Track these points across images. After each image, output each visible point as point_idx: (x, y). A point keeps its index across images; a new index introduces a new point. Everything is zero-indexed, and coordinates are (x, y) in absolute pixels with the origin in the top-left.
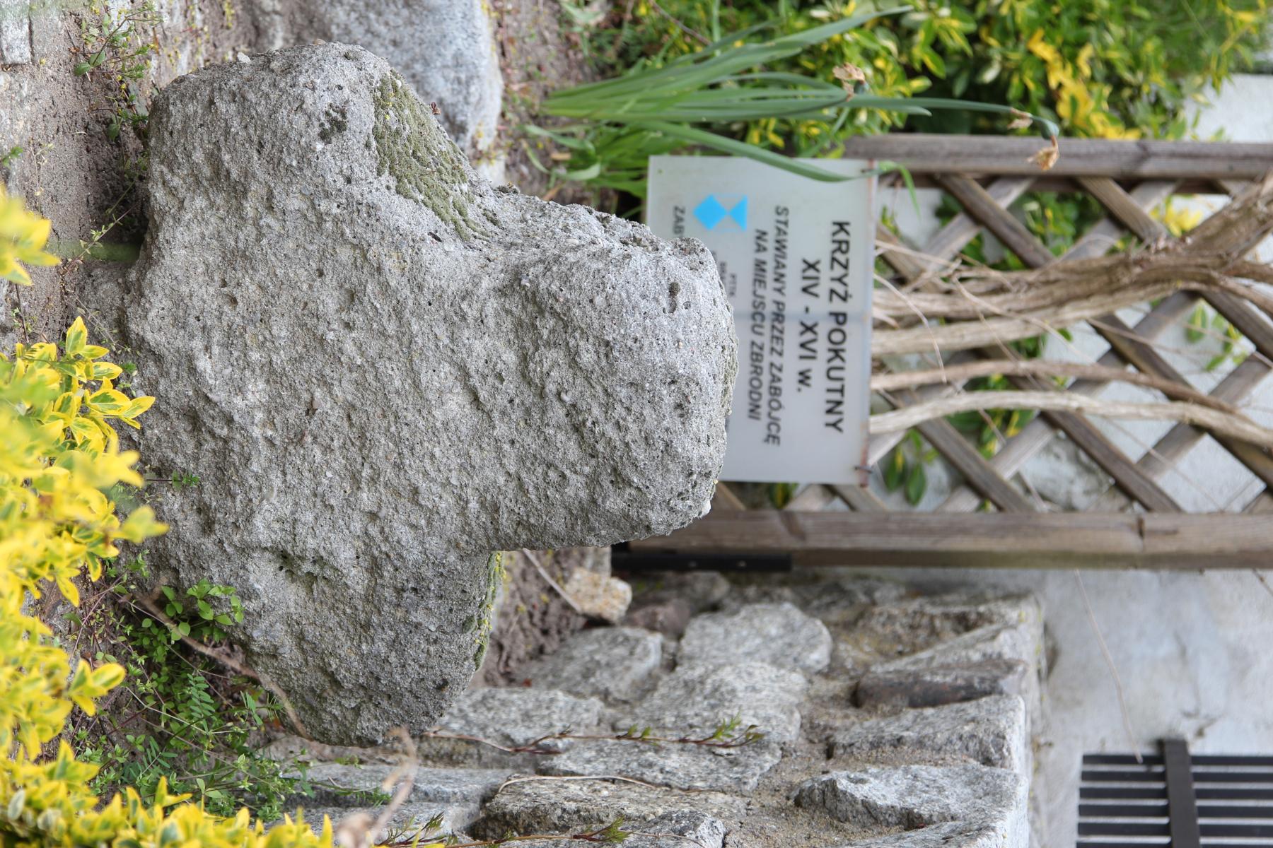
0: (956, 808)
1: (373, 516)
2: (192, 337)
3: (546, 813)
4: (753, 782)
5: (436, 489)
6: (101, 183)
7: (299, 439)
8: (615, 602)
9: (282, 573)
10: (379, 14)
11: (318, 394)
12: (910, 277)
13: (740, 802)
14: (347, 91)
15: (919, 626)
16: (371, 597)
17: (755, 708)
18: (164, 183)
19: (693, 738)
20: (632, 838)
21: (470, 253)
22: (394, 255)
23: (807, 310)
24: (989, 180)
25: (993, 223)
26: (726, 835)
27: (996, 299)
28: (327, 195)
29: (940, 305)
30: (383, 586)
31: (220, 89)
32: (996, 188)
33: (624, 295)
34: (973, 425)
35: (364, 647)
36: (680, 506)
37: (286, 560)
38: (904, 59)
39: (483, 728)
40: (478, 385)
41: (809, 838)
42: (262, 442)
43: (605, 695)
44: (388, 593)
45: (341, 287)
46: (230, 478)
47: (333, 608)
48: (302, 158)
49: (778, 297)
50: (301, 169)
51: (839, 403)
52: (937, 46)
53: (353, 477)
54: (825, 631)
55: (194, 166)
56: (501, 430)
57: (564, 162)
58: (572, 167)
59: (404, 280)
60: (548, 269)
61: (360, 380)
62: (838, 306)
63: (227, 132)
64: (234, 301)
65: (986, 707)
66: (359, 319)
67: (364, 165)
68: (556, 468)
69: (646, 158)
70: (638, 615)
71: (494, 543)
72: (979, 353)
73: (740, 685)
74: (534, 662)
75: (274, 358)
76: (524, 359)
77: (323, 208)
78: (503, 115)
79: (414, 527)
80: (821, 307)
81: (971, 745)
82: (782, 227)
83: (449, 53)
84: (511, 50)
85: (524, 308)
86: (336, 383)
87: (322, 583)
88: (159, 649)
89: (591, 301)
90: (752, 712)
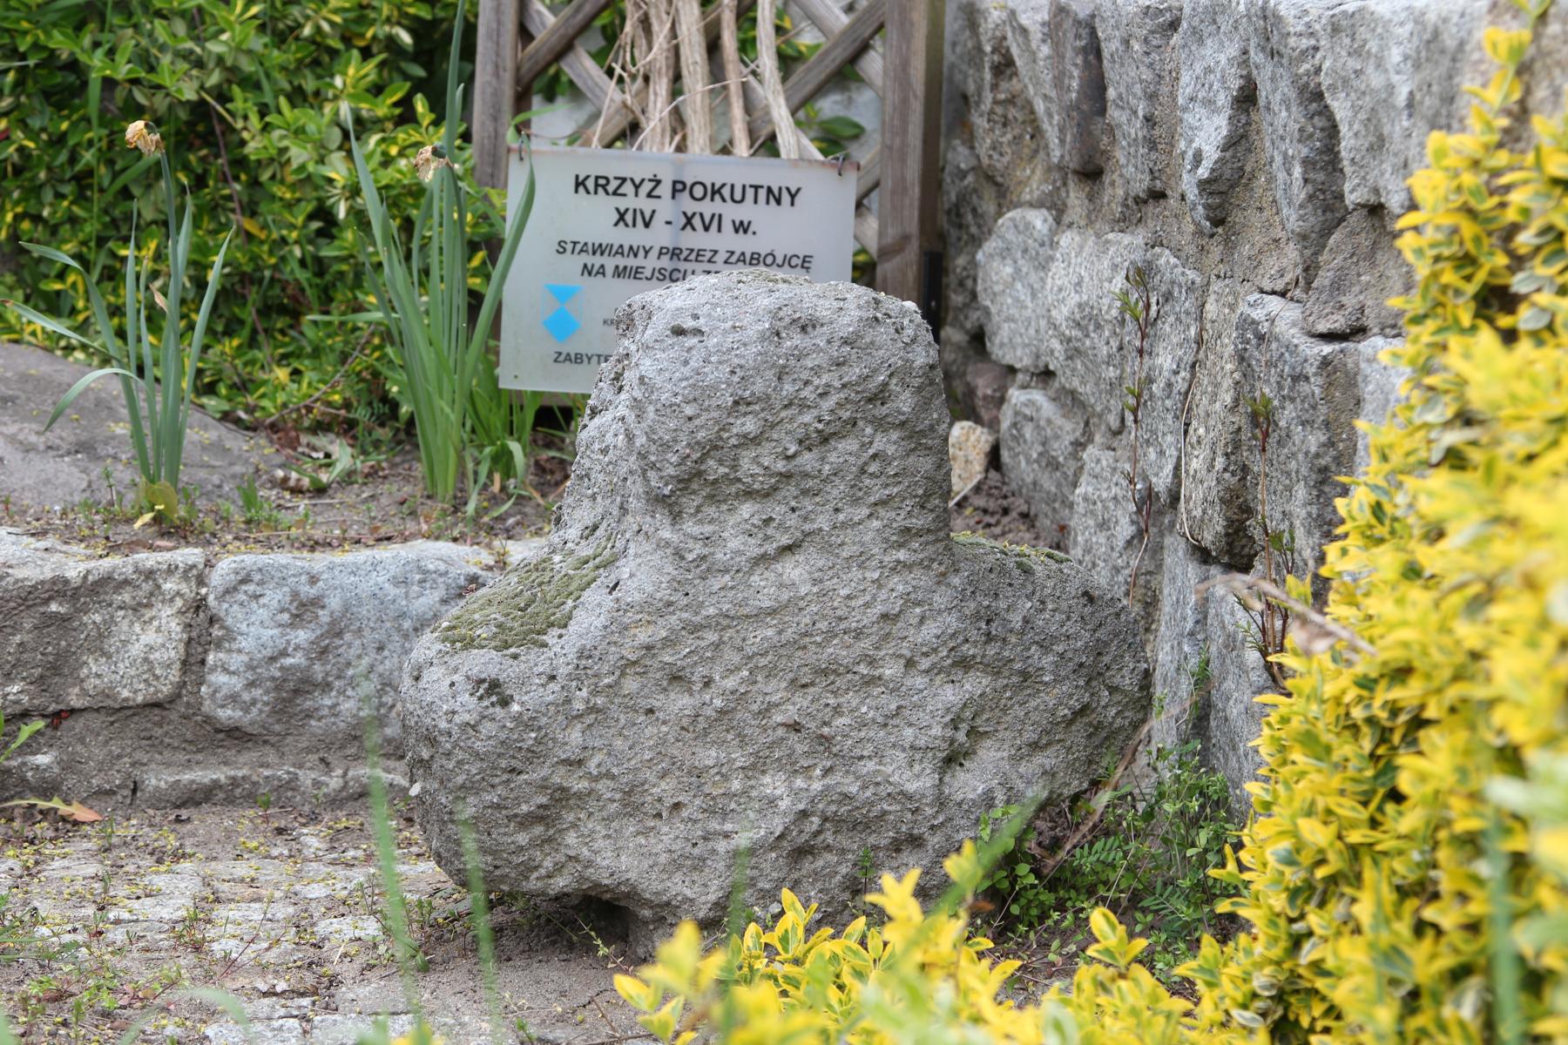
0: (1233, 50)
1: (910, 663)
2: (714, 852)
3: (1228, 489)
4: (1191, 274)
5: (883, 594)
6: (544, 947)
7: (825, 740)
8: (973, 438)
9: (967, 764)
10: (349, 664)
11: (779, 718)
12: (630, 117)
13: (1216, 286)
14: (455, 678)
15: (1005, 117)
16: (995, 669)
17: (1101, 281)
18: (549, 877)
19: (1138, 343)
20: (1266, 390)
21: (631, 551)
22: (633, 631)
23: (668, 223)
24: (525, 34)
25: (571, 31)
26: (1262, 291)
27: (655, 27)
28: (568, 701)
29: (661, 86)
30: (984, 656)
31: (451, 813)
32: (532, 29)
33: (684, 384)
34: (788, 61)
35: (1047, 679)
36: (910, 332)
37: (953, 759)
38: (389, 125)
39: (1117, 570)
40: (775, 545)
41: (1260, 209)
42: (827, 781)
43: (1079, 445)
44: (991, 651)
45: (665, 690)
46: (865, 816)
47: (1005, 710)
48: (528, 727)
49: (654, 253)
50: (540, 728)
51: (770, 190)
52: (377, 90)
53: (867, 683)
54: (1009, 215)
55: (533, 844)
56: (822, 522)
57: (502, 480)
58: (508, 471)
59: (661, 621)
60: (653, 466)
61: (765, 673)
62: (665, 190)
63: (498, 807)
64: (677, 806)
65: (1109, 31)
66: (701, 671)
67: (535, 661)
68: (866, 464)
69: (499, 391)
70: (986, 416)
71: (942, 534)
72: (713, 47)
73: (1074, 299)
74: (1037, 524)
75: (738, 764)
76: (749, 494)
77: (581, 706)
78: (455, 540)
79: (922, 620)
80: (666, 208)
81: (1155, 42)
82: (578, 247)
83: (392, 591)
84: (383, 532)
85: (694, 492)
86: (768, 698)
87: (978, 721)
88: (1042, 897)
89: (690, 419)
90: (1106, 284)
